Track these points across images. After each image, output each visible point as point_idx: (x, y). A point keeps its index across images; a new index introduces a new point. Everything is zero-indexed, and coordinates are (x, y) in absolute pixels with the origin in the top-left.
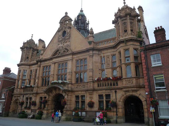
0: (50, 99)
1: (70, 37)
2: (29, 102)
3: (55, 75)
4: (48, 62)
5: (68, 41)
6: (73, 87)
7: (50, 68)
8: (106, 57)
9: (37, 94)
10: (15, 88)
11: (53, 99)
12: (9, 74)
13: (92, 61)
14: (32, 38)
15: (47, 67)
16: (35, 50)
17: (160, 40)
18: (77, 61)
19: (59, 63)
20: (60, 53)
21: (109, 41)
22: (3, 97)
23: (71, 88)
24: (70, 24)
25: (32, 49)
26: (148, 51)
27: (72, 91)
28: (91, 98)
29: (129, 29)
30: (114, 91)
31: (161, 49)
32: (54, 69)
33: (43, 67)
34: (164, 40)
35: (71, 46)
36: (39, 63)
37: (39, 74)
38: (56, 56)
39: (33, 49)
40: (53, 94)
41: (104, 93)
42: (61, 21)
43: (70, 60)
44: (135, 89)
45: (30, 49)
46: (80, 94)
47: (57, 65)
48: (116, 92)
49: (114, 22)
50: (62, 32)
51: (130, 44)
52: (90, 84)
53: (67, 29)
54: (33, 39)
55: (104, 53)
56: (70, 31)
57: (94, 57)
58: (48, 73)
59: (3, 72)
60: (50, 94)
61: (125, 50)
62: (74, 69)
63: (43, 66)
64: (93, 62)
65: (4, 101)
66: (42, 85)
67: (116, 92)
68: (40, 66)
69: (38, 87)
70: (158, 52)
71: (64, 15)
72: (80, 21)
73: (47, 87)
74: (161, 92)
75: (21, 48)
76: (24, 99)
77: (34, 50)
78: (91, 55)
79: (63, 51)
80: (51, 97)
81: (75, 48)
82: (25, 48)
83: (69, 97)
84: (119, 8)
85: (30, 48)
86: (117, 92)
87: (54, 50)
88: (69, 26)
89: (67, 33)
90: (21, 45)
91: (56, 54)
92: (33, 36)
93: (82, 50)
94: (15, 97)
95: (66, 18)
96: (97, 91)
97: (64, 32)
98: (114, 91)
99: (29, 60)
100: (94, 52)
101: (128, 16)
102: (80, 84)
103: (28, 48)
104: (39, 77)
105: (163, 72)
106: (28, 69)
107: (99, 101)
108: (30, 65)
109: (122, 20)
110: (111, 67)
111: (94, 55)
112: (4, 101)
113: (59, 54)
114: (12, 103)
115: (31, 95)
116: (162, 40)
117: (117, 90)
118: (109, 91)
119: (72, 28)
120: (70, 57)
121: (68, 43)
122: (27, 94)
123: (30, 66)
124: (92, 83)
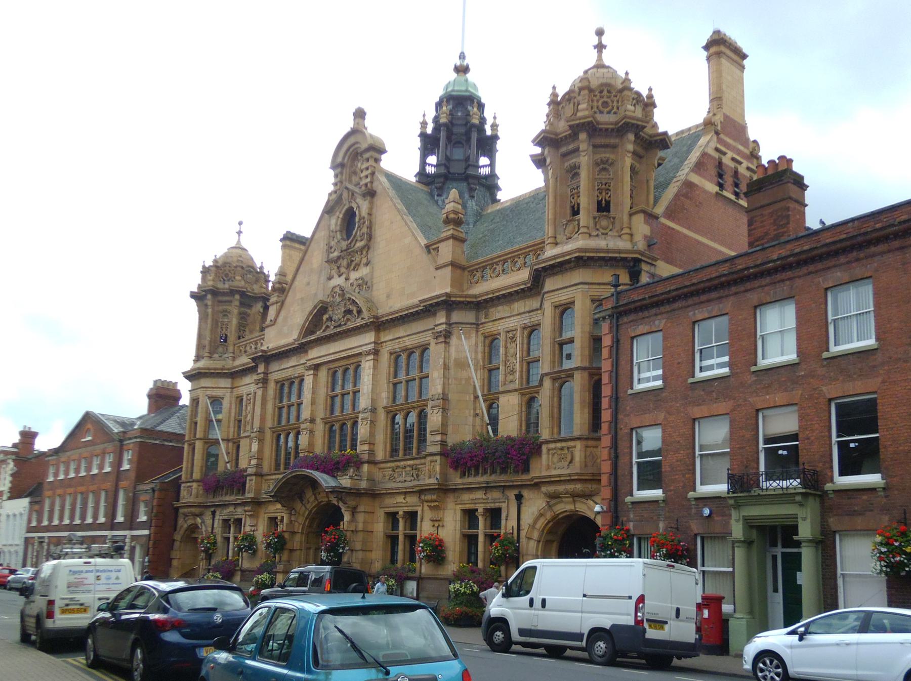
0: (298, 528)
1: (370, 237)
2: (406, 536)
3: (318, 420)
4: (293, 361)
5: (364, 260)
6: (378, 475)
7: (428, 361)
8: (502, 338)
9: (257, 503)
10: (183, 478)
11: (310, 526)
12: (176, 408)
13: (441, 361)
14: (600, 58)
15: (410, 352)
16: (256, 298)
17: (767, 234)
18: (396, 356)
19: (332, 366)
20: (330, 319)
21: (518, 256)
22: (143, 518)
23: (371, 480)
24: (369, 171)
25: (237, 297)
26: (625, 319)
27: (373, 494)
28: (436, 524)
29: (586, 202)
30: (512, 494)
31: (668, 312)
32: (313, 393)
33: (279, 385)
34: (783, 234)
36: (261, 369)
37: (263, 419)
38: (319, 334)
39: (243, 294)
40: (309, 506)
41: (479, 501)
42: (339, 160)
43: (368, 353)
44: (579, 487)
45: (230, 295)
46: (402, 504)
47: (323, 374)
48: (519, 498)
49: (539, 162)
50: (339, 214)
52: (431, 462)
53: (359, 200)
54: (607, 61)
55: (498, 316)
56: (371, 209)
57: (454, 340)
58: (416, 389)
59: (146, 401)
60: (298, 506)
61: (561, 309)
62: (384, 395)
63: (277, 382)
64: (455, 360)
65: (146, 532)
66: (394, 451)
67: (519, 498)
68: (265, 382)
69: (259, 475)
70: (657, 322)
71: (348, 124)
72: (443, 135)
73: (280, 476)
74: (646, 505)
75: (193, 296)
76: (216, 526)
77: (247, 299)
78: (439, 329)
79: (343, 309)
80: (301, 520)
81: (388, 296)
82: (209, 296)
83: (361, 518)
84: (554, 88)
85: (232, 292)
86: (523, 501)
87: (309, 306)
88: (366, 185)
89: (357, 219)
90: (194, 282)
91: (320, 324)
92: (605, 40)
93: (407, 309)
94: (185, 515)
95: (352, 140)
96: (456, 494)
97: (350, 215)
98: (512, 494)
99: (231, 349)
100: (456, 316)
101: (583, 136)
102: (402, 463)
103: (224, 294)
104: (261, 431)
105: (661, 416)
106: (228, 395)
107: (388, 536)
108: (235, 375)
109: (564, 155)
110: (517, 385)
111: (455, 331)
112: (146, 532)
113: (328, 327)
114: (177, 544)
115: (240, 510)
116: (772, 234)
117: (526, 493)
118: (496, 494)
120: (368, 338)
121: (363, 271)
122: (224, 506)
123: (233, 378)
124: (438, 458)
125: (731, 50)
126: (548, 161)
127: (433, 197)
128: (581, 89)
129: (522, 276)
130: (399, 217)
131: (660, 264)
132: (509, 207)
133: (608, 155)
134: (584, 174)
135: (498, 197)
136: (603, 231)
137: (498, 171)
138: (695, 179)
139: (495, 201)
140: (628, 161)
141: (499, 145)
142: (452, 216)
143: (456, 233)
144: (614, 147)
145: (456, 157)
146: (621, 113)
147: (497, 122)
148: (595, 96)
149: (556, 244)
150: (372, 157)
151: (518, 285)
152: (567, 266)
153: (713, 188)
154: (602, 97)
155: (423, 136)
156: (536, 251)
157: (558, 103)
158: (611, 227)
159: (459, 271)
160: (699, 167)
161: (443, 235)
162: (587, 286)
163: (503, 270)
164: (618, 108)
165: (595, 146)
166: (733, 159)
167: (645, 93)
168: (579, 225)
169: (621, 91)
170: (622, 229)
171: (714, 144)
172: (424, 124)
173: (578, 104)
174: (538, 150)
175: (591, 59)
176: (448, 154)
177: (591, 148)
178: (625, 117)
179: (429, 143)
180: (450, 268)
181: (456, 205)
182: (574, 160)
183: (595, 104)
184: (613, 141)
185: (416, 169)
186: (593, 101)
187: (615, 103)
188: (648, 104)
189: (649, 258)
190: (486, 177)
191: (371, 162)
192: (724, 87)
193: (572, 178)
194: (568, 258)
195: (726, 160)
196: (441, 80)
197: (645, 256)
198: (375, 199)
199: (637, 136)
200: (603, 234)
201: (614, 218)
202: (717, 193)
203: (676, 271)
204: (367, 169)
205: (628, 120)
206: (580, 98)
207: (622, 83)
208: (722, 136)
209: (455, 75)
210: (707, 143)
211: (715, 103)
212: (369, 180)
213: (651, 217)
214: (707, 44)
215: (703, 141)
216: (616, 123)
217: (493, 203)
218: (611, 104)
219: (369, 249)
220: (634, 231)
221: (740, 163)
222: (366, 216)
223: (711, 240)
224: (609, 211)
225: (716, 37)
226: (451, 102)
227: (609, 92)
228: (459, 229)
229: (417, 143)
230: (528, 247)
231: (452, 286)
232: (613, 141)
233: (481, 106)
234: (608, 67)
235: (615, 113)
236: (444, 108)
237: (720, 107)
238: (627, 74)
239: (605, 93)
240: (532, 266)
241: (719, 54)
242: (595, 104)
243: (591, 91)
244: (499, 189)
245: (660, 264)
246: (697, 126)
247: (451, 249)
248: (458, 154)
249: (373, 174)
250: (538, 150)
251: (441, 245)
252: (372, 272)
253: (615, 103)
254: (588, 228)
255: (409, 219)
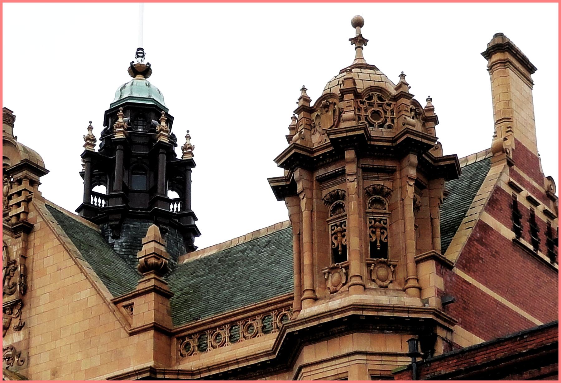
1: (25, 289)
5: (15, 322)
14: (359, 56)
24: (22, 198)
29: (354, 243)
35: (32, 361)
49: (283, 190)
51: (350, 350)
54: (370, 55)
56: (26, 249)
72: (118, 155)
84: (304, 89)
88: (18, 216)
92: (365, 32)
101: (350, 154)
109: (322, 180)
119: (37, 226)
125: (518, 60)
126: (300, 187)
127: (106, 239)
128: (343, 92)
129: (267, 342)
130: (71, 262)
131: (458, 329)
132: (215, 256)
133: (382, 183)
134: (352, 206)
135: (195, 244)
136: (381, 283)
137: (195, 207)
138: (490, 220)
139: (192, 248)
140: (410, 191)
141: (195, 174)
142: (152, 261)
143: (158, 284)
144: (391, 172)
145: (136, 187)
146: (399, 127)
147: (192, 142)
148: (362, 103)
149: (316, 299)
150: (26, 177)
151: (256, 356)
152: (335, 329)
153: (510, 235)
154: (371, 105)
155: (87, 156)
156: (279, 310)
157: (311, 110)
158: (391, 278)
159: (164, 338)
160: (492, 205)
161: (141, 287)
162: (364, 357)
163: (264, 327)
164: (393, 121)
165: (366, 170)
166: (529, 199)
167: (424, 104)
168: (347, 274)
169: (395, 98)
170: (407, 281)
171: (506, 178)
172: (90, 140)
173: (340, 113)
174: (280, 172)
175: (348, 56)
176: (126, 181)
177: (360, 171)
178: (407, 131)
179: (96, 166)
180: (152, 333)
181: (157, 246)
182: (336, 188)
183: (363, 113)
184: (389, 164)
185: (80, 201)
186: (359, 110)
187: (389, 115)
188: (429, 118)
189: (445, 321)
190: (179, 216)
191: (25, 185)
192: (513, 105)
193: (334, 211)
194: (337, 317)
195: (521, 198)
196: (110, 85)
197: (441, 318)
198: (32, 236)
199: (421, 159)
200: (381, 286)
201: (394, 266)
202: (514, 240)
203: (479, 341)
204: (19, 194)
205: (412, 137)
206: (342, 105)
207: (396, 89)
208: (514, 167)
209: (130, 79)
210: (498, 175)
211: (503, 125)
212: (22, 209)
213: (444, 265)
214: (488, 50)
215: (493, 172)
216: (394, 140)
217: (188, 252)
218: (383, 115)
219: (23, 306)
220: (423, 284)
221: (536, 204)
222: (18, 260)
223: (511, 301)
224: (386, 257)
225: (499, 41)
226: (129, 112)
227: (380, 98)
228: (162, 279)
229: (78, 165)
230: (268, 305)
231: (155, 359)
232: (389, 164)
233: (170, 120)
234: (373, 68)
235: (389, 127)
236: (120, 120)
237: (509, 130)
238: (403, 76)
239: (375, 100)
240: (282, 331)
241: (504, 63)
242: (363, 113)
243: (357, 95)
244: (197, 233)
245: (458, 329)
246: (487, 151)
247: (152, 305)
248: (139, 183)
249: (28, 201)
250: (280, 172)
251: (137, 301)
252: (28, 339)
253: (389, 115)
254: (361, 277)
255: (85, 264)
